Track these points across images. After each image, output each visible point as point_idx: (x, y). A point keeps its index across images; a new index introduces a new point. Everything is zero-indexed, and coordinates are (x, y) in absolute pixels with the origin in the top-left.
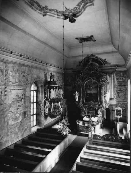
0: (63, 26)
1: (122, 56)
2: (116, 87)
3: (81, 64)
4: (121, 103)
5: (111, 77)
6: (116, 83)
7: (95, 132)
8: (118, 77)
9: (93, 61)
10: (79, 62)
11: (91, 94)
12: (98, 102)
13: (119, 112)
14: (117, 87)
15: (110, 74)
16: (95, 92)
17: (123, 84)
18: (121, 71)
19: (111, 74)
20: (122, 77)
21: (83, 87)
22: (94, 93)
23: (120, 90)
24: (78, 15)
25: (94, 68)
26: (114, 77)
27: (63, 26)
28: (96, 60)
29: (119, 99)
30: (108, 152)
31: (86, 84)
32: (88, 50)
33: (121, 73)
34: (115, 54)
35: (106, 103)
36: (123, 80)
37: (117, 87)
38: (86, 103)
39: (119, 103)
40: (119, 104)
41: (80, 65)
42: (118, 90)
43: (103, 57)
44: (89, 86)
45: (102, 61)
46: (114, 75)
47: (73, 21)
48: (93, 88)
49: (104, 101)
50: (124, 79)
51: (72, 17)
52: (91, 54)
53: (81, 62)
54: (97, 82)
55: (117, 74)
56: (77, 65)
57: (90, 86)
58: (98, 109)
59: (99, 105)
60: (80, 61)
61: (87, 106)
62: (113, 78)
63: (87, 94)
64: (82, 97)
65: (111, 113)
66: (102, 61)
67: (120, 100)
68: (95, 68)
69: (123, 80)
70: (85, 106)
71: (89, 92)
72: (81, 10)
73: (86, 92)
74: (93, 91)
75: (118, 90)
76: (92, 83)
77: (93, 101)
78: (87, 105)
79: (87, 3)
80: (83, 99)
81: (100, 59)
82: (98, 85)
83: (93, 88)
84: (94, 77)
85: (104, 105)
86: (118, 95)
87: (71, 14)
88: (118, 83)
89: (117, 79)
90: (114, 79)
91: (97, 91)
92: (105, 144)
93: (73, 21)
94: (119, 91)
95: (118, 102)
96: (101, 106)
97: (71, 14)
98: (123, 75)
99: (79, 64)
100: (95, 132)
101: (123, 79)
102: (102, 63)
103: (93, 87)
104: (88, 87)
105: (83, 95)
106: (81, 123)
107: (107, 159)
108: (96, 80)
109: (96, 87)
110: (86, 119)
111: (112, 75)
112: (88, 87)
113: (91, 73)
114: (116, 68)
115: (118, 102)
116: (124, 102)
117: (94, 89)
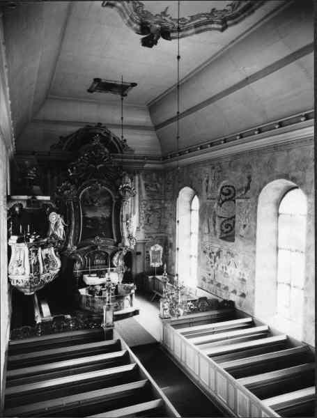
0: (179, 57)
1: (160, 140)
2: (144, 204)
3: (64, 142)
4: (154, 236)
5: (135, 182)
6: (144, 194)
7: (131, 305)
8: (147, 182)
9: (101, 141)
10: (61, 137)
11: (94, 220)
12: (113, 238)
13: (156, 256)
14: (145, 203)
15: (132, 174)
16: (106, 215)
17: (156, 198)
18: (154, 170)
19: (135, 175)
20: (155, 182)
21: (76, 204)
22: (103, 218)
23: (152, 209)
24: (172, 35)
25: (103, 157)
26: (139, 180)
27: (179, 57)
28: (107, 140)
29: (148, 227)
30: (213, 333)
31: (83, 195)
32: (106, 113)
33: (154, 175)
34: (146, 132)
35: (130, 237)
36: (157, 188)
37: (145, 203)
38: (85, 242)
39: (149, 237)
40: (150, 239)
41: (61, 147)
42: (148, 210)
43: (116, 133)
44: (92, 200)
45: (117, 142)
46: (141, 177)
47: (149, 42)
48: (99, 204)
49: (126, 235)
50: (158, 186)
51: (150, 35)
52: (97, 122)
53: (68, 137)
54: (109, 190)
55: (145, 176)
56: (53, 145)
57: (95, 200)
58: (113, 255)
59: (116, 245)
60: (64, 136)
61: (88, 250)
62: (137, 183)
63: (86, 219)
64: (75, 228)
65: (134, 260)
66: (117, 142)
67: (152, 230)
68: (105, 158)
69: (157, 188)
70: (82, 249)
71: (90, 215)
72: (187, 29)
73: (84, 214)
74: (101, 213)
75: (148, 210)
76: (98, 192)
77: (101, 236)
78: (86, 248)
79: (212, 22)
80: (76, 235)
81: (114, 138)
82: (111, 198)
83: (99, 204)
84: (103, 178)
85: (127, 243)
86: (148, 220)
87: (158, 26)
88: (148, 195)
89: (146, 186)
90: (139, 185)
91: (111, 212)
92: (191, 321)
93: (149, 42)
94: (150, 211)
95: (147, 234)
96: (120, 245)
97: (158, 26)
98: (157, 178)
99: (60, 143)
100: (131, 305)
101: (156, 185)
102: (117, 147)
103: (100, 202)
104: (88, 203)
105: (78, 221)
106: (83, 291)
107: (226, 344)
108: (106, 185)
109: (109, 203)
110: (91, 280)
111: (137, 178)
112: (89, 204)
113: (96, 169)
114: (146, 163)
115: (147, 234)
116: (157, 233)
117: (103, 208)
